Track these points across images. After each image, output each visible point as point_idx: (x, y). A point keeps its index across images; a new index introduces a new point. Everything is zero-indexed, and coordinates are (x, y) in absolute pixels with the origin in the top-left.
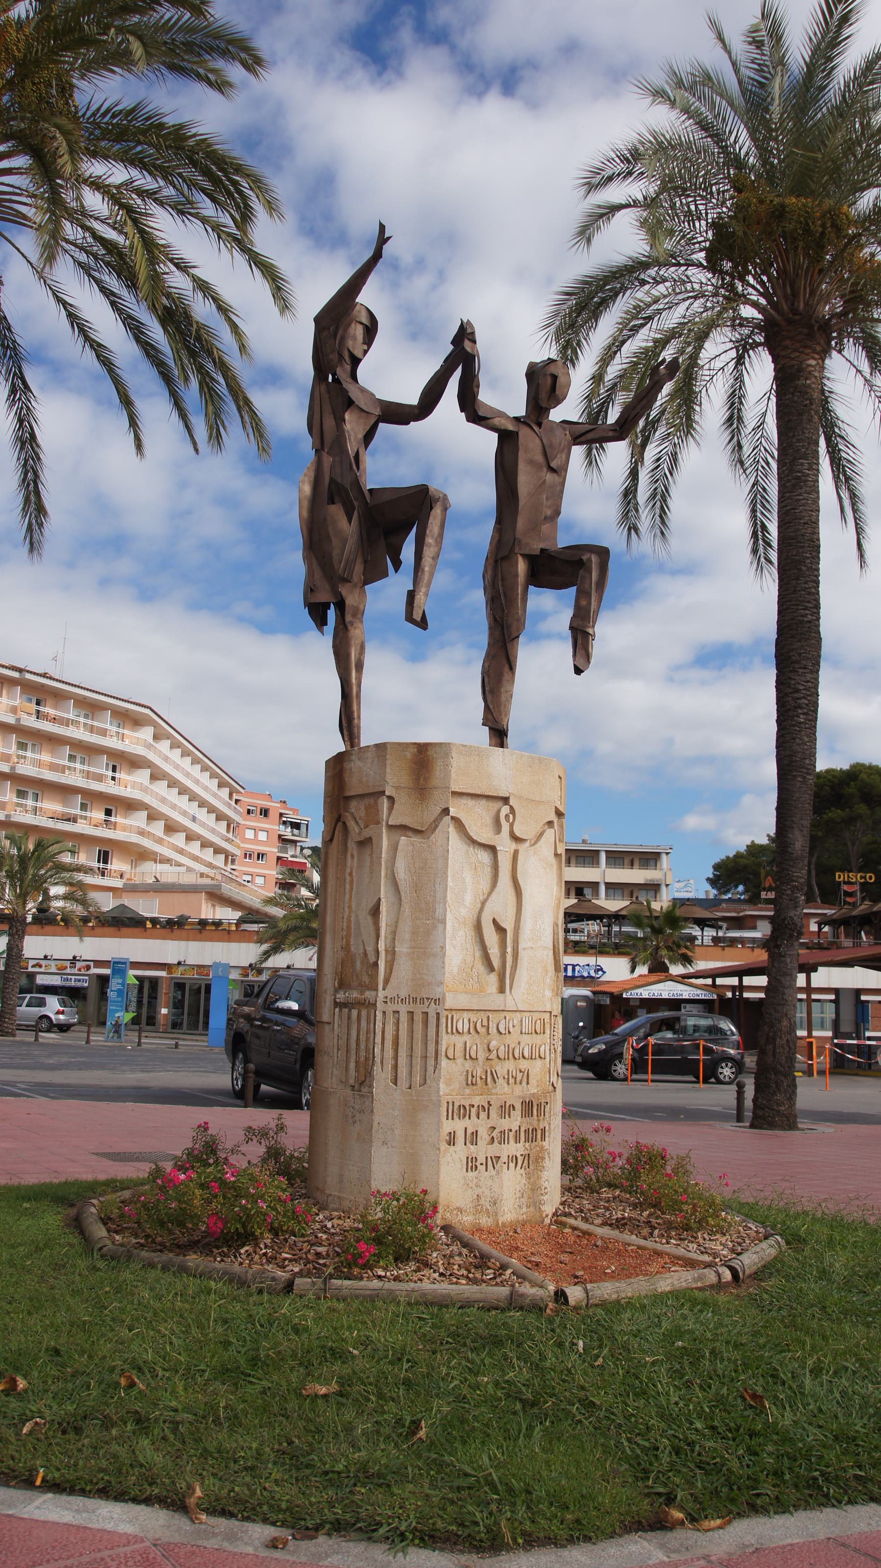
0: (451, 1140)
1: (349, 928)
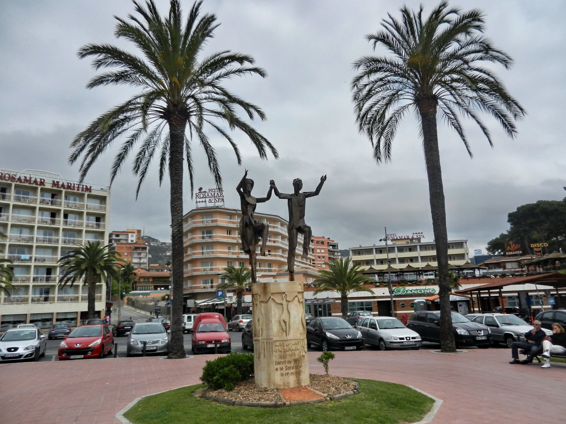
0: (277, 370)
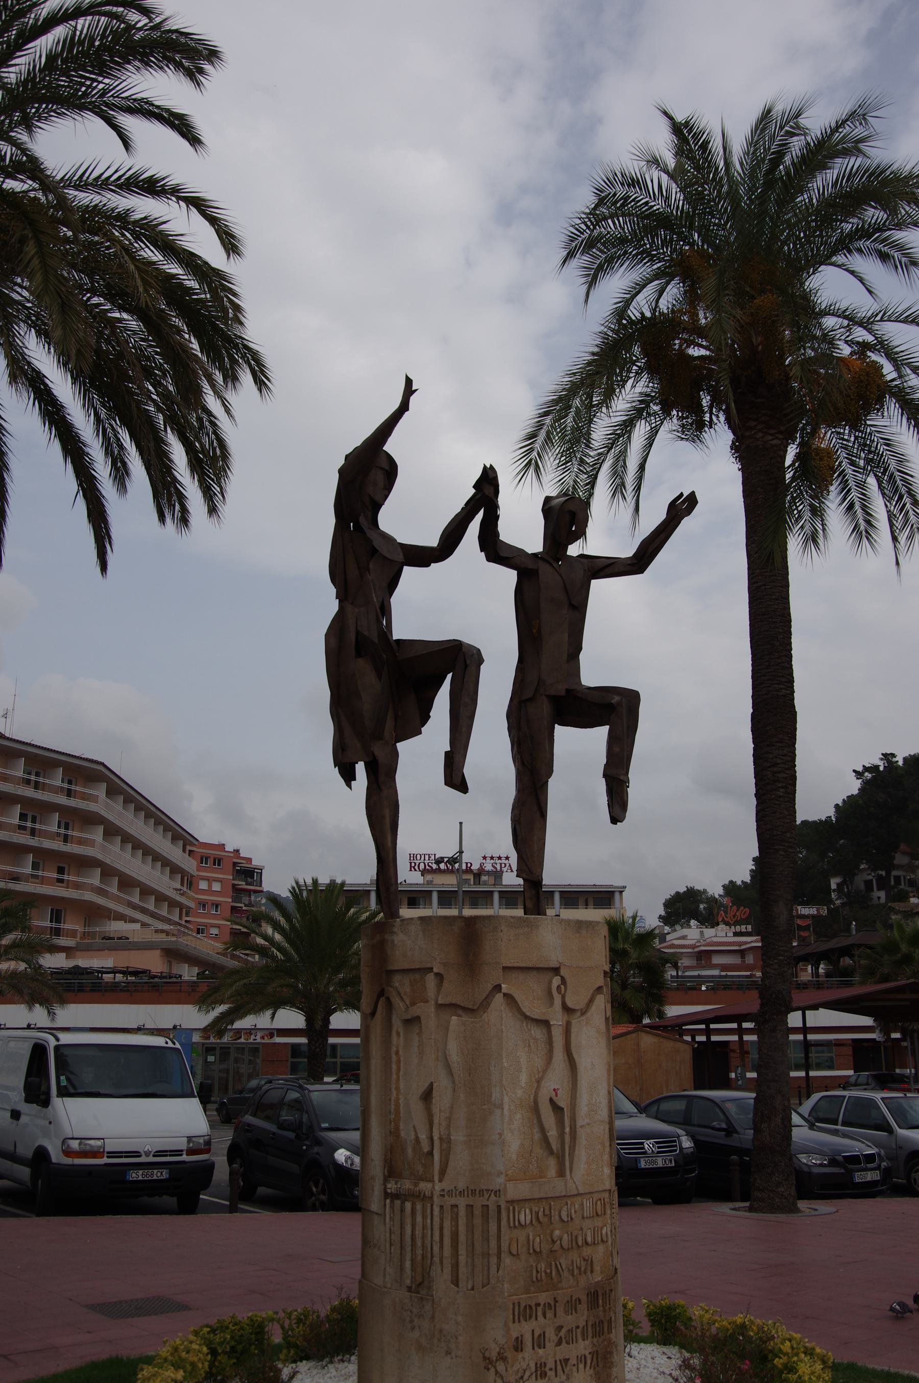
1: (397, 1111)
